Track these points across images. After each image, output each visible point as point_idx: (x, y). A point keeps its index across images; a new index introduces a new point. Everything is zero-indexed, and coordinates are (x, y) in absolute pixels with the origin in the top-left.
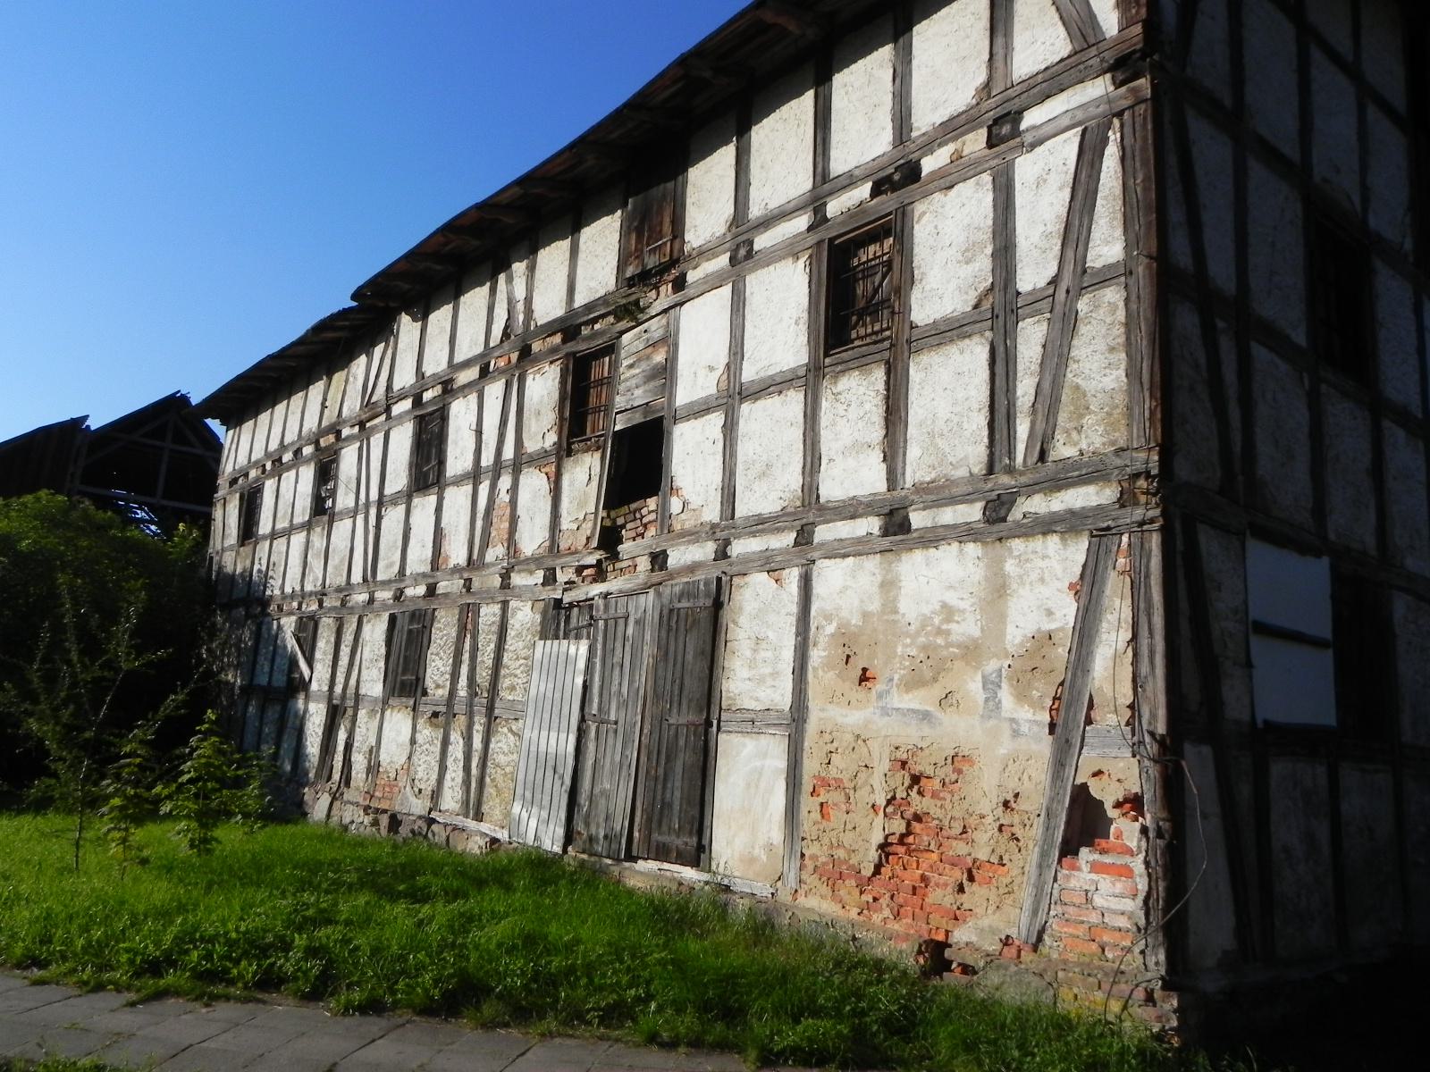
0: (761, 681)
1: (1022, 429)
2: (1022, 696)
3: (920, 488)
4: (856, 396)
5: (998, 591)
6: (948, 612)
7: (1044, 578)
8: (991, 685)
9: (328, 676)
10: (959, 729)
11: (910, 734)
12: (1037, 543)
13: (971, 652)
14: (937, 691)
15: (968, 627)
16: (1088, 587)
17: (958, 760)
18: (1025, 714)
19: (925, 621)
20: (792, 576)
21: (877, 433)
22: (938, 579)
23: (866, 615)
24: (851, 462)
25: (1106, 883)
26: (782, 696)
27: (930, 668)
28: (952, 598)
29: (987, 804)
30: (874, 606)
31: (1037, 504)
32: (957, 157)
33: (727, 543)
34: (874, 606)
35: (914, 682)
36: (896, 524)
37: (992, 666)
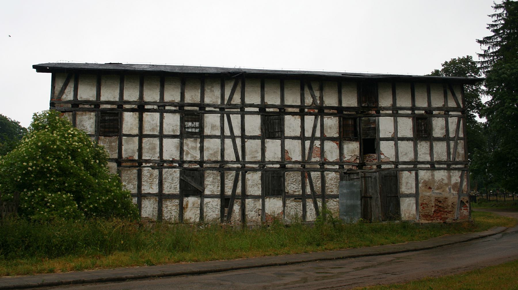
0: (409, 189)
1: (451, 156)
2: (454, 190)
3: (436, 161)
4: (191, 201)
5: (449, 177)
6: (443, 179)
7: (456, 177)
8: (450, 189)
9: (394, 153)
10: (445, 195)
11: (439, 196)
12: (455, 171)
13: (446, 185)
14: (442, 190)
15: (446, 181)
16: (461, 177)
17: (446, 198)
18: (454, 192)
19: (439, 180)
20: (413, 173)
21: (428, 152)
22: (440, 175)
23: (429, 179)
24: (424, 155)
25: (465, 211)
26: (413, 191)
27: (440, 187)
28: (443, 177)
29: (450, 204)
30: (431, 178)
31: (454, 166)
32: (439, 113)
33: (397, 165)
34: (431, 178)
35: (437, 189)
36: (365, 197)
37: (450, 186)
